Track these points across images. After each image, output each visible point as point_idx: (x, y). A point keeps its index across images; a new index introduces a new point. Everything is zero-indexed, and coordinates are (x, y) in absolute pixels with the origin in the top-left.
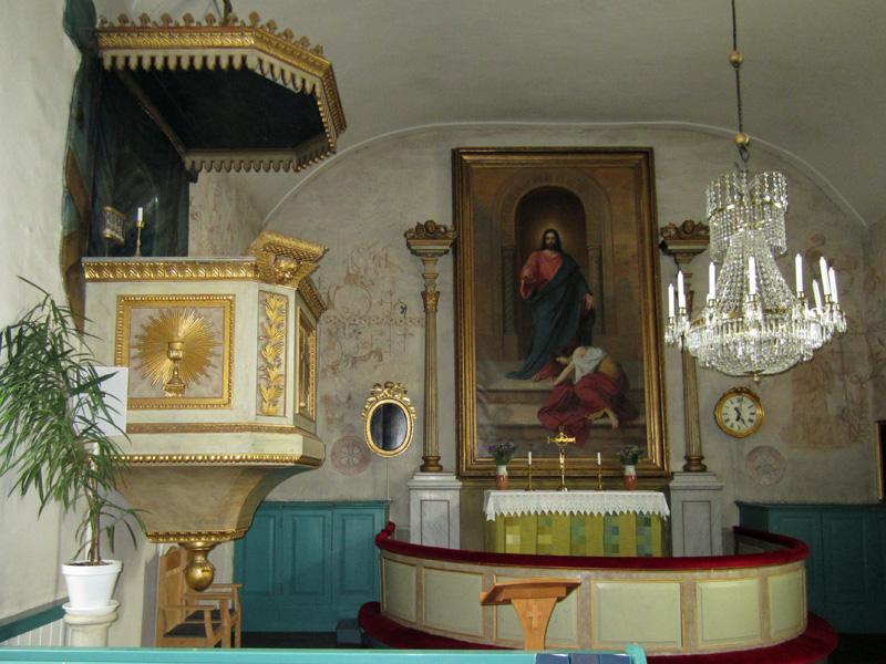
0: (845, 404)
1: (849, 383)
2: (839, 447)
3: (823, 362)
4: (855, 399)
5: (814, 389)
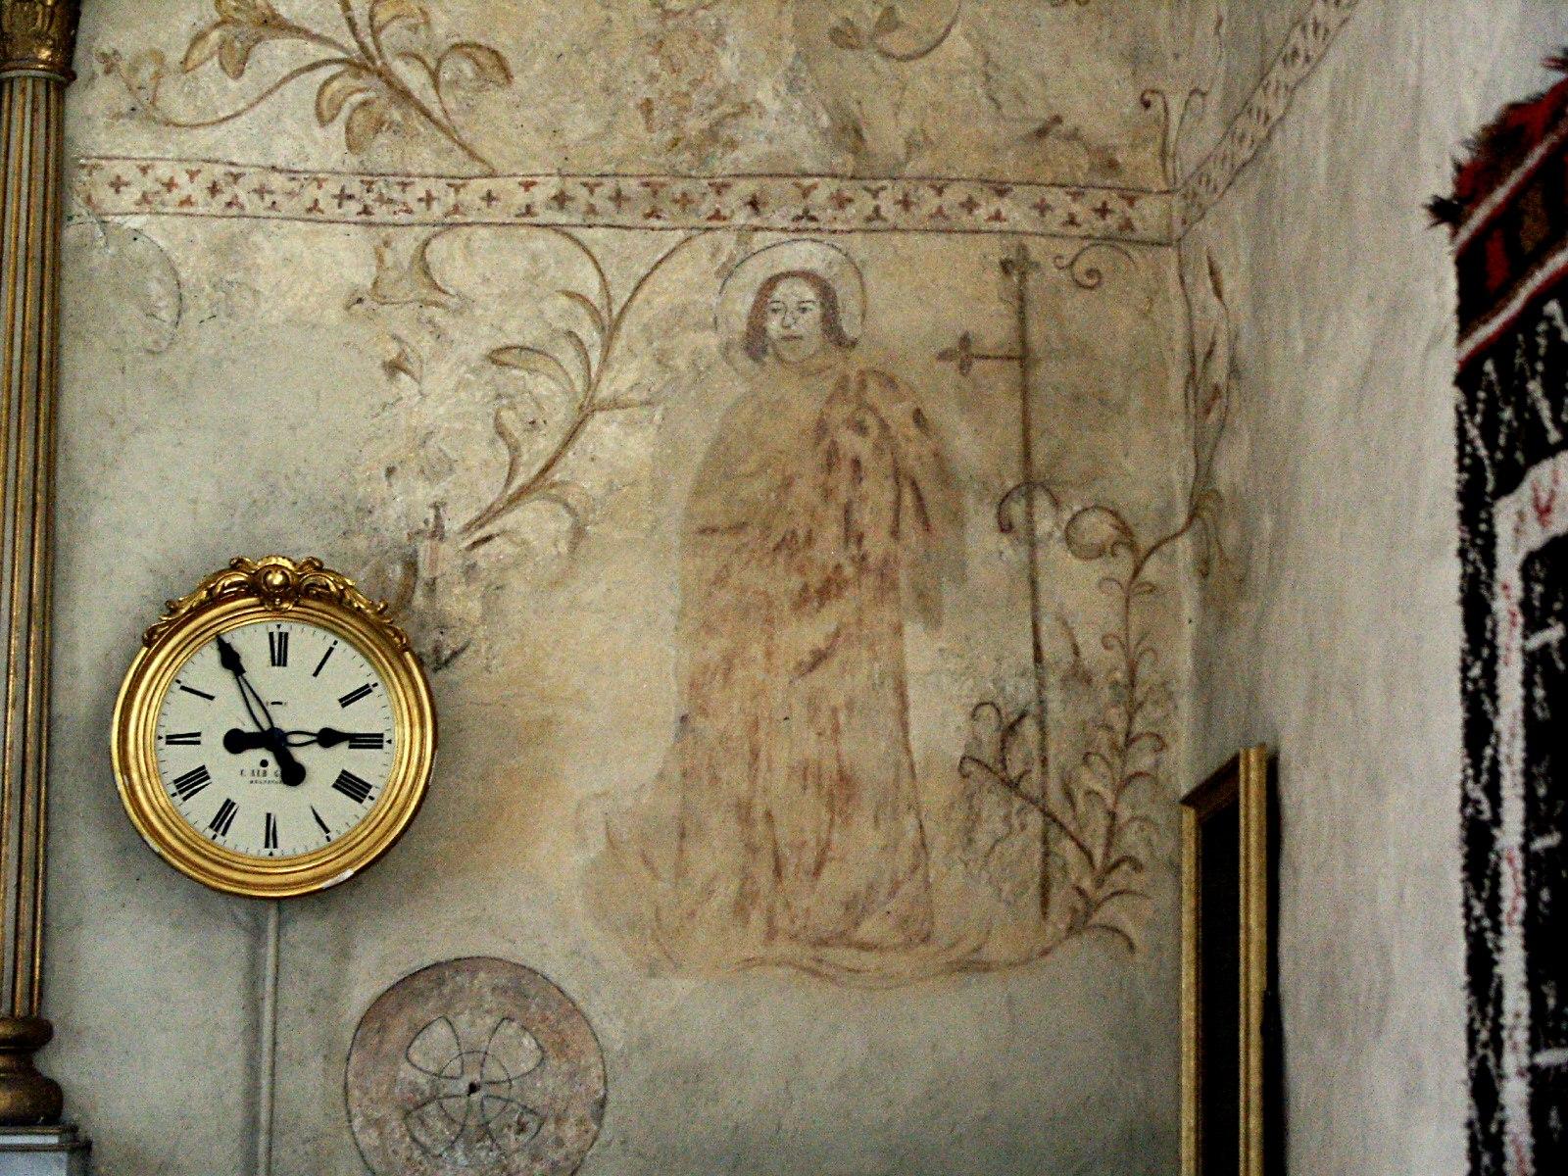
0: (1023, 691)
1: (1056, 556)
2: (973, 965)
3: (898, 413)
4: (1092, 651)
5: (829, 589)
